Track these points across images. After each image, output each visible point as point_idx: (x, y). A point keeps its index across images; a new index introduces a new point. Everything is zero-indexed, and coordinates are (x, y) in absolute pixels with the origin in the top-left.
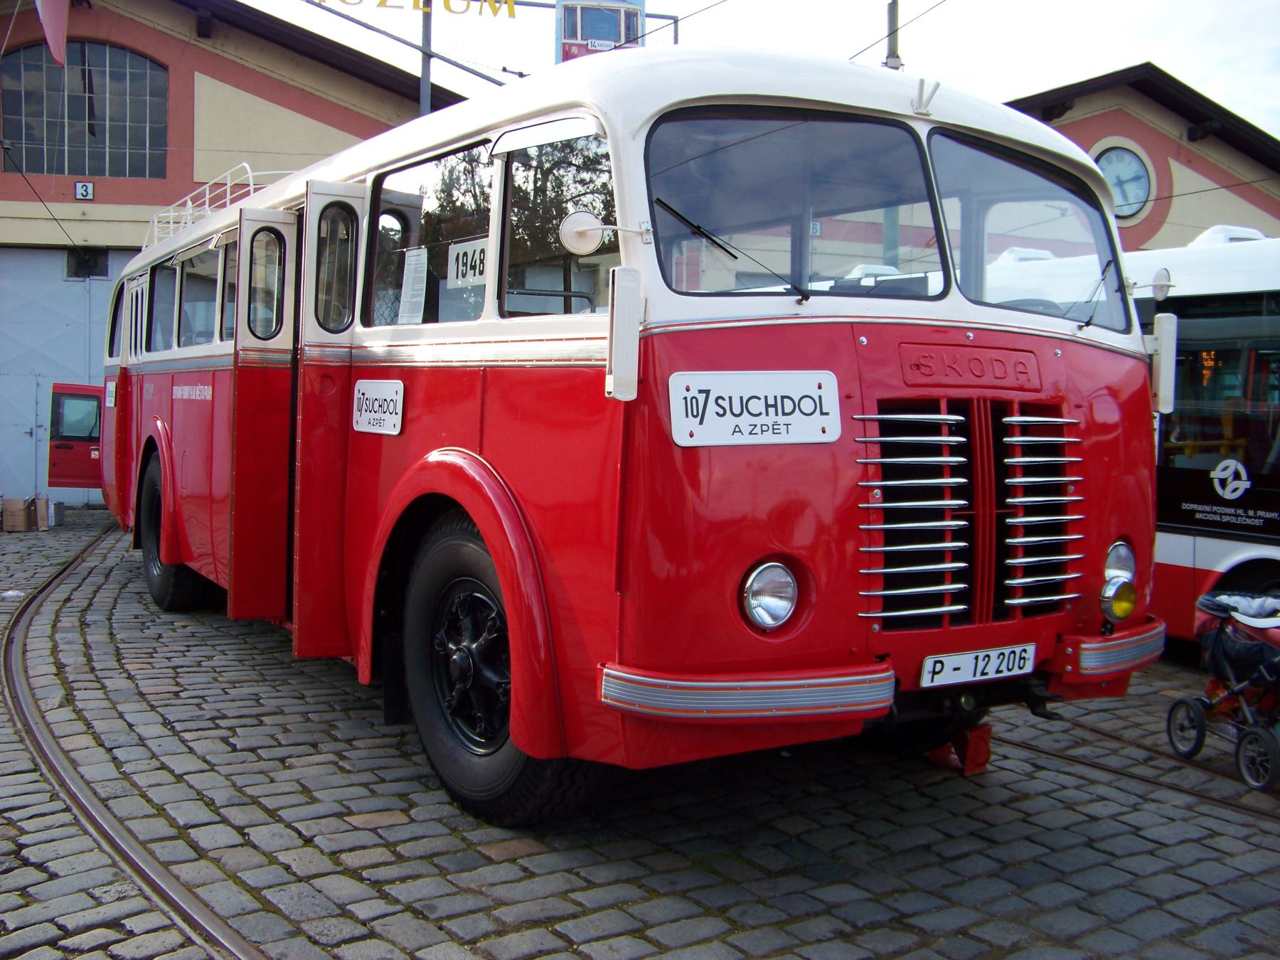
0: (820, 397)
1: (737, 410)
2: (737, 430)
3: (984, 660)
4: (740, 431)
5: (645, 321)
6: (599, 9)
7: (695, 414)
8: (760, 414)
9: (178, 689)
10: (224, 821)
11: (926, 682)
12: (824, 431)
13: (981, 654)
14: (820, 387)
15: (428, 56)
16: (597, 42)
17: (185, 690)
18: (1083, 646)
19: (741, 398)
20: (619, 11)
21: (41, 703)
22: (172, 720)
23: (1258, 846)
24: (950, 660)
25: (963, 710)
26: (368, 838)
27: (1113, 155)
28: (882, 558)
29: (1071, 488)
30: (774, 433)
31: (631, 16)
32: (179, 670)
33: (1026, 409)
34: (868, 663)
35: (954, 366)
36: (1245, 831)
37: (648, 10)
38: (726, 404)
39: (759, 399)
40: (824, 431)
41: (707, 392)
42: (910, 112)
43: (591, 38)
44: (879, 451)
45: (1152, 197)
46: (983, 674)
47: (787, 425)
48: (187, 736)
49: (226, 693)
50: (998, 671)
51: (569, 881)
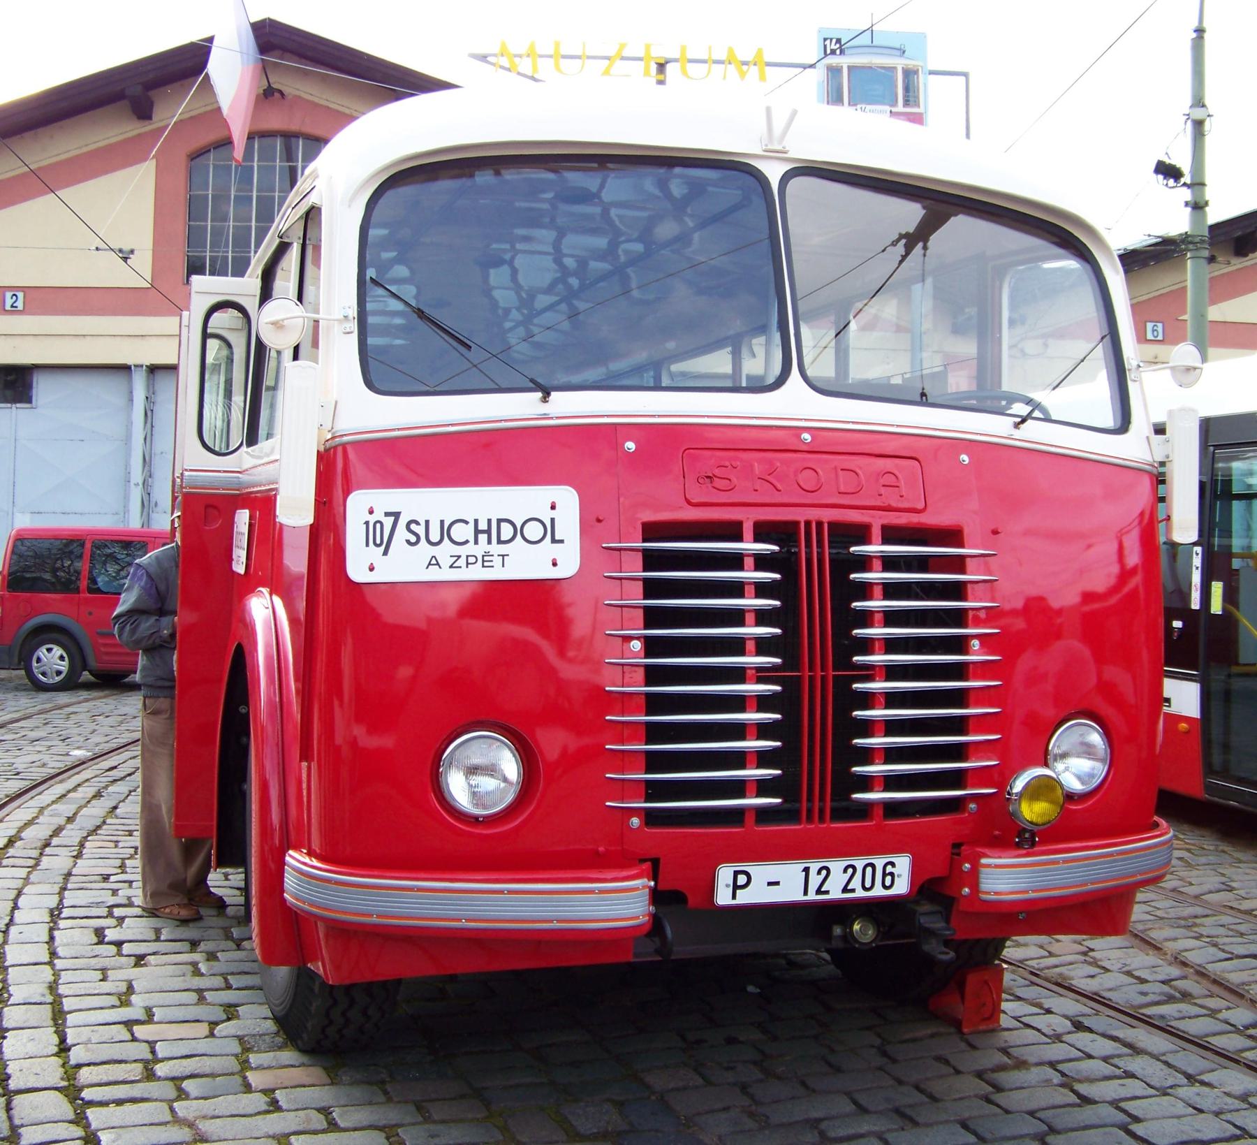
0: (553, 520)
1: (435, 537)
2: (434, 562)
3: (819, 872)
4: (438, 564)
5: (332, 428)
6: (870, 68)
7: (378, 542)
8: (467, 542)
11: (723, 897)
12: (555, 564)
13: (814, 866)
14: (553, 507)
18: (984, 861)
19: (442, 522)
20: (895, 68)
21: (242, 884)
24: (761, 872)
25: (856, 941)
28: (643, 731)
29: (975, 644)
30: (483, 566)
31: (909, 74)
33: (890, 536)
34: (622, 866)
35: (769, 478)
37: (932, 66)
38: (420, 530)
39: (466, 522)
40: (555, 564)
41: (396, 515)
42: (759, 151)
43: (860, 104)
44: (753, 591)
46: (819, 892)
47: (503, 556)
49: (227, 879)
50: (845, 890)
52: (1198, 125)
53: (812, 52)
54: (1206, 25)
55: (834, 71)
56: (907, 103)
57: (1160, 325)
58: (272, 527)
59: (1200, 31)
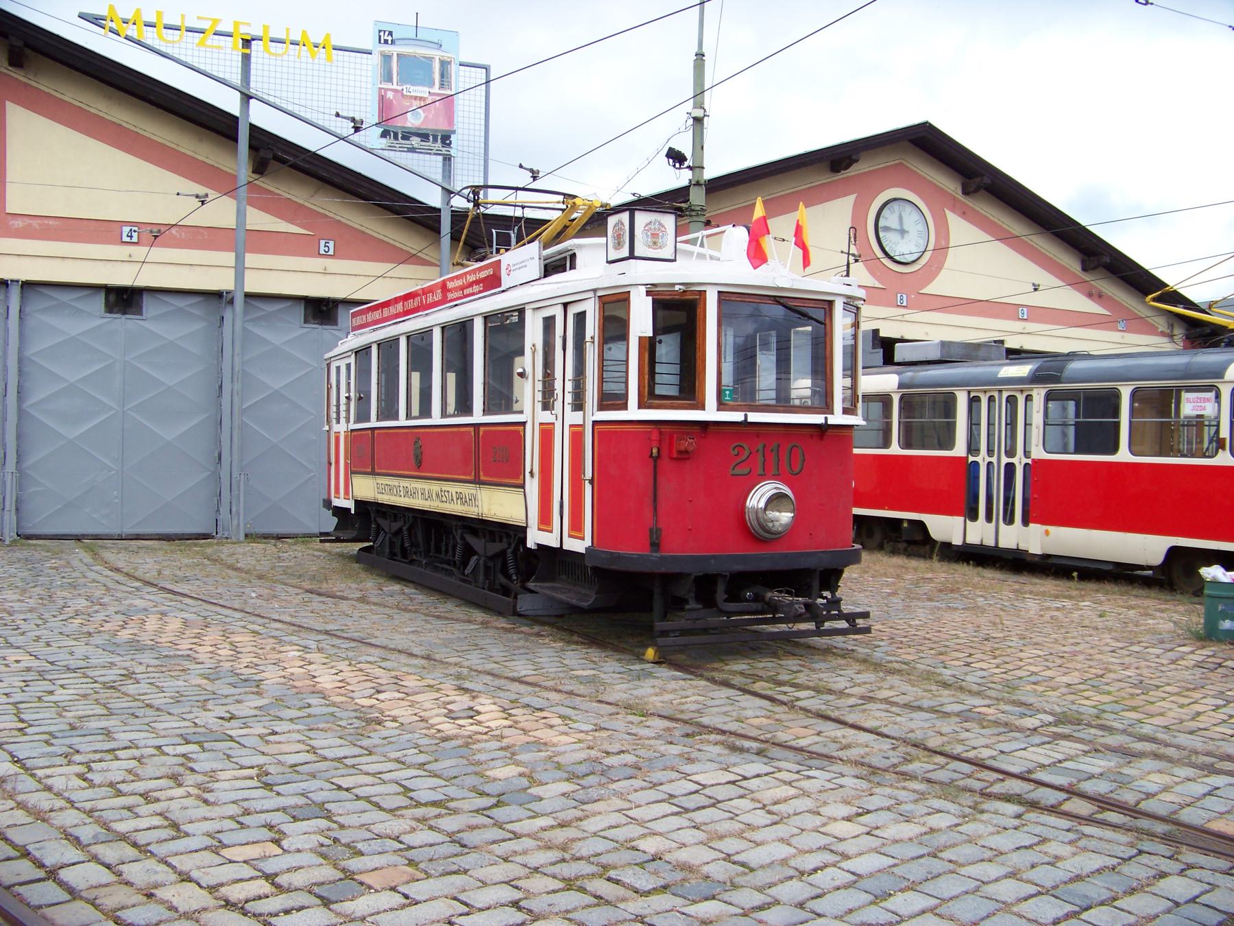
9: (21, 725)
10: (95, 858)
15: (247, 98)
16: (412, 88)
17: (31, 726)
22: (21, 758)
23: (1085, 849)
26: (247, 872)
27: (895, 205)
31: (444, 64)
32: (20, 706)
36: (1071, 836)
43: (406, 83)
45: (931, 247)
48: (40, 773)
51: (450, 906)
52: (698, 121)
53: (367, 40)
54: (704, 50)
55: (387, 58)
56: (442, 86)
57: (905, 296)
58: (496, 480)
59: (700, 55)
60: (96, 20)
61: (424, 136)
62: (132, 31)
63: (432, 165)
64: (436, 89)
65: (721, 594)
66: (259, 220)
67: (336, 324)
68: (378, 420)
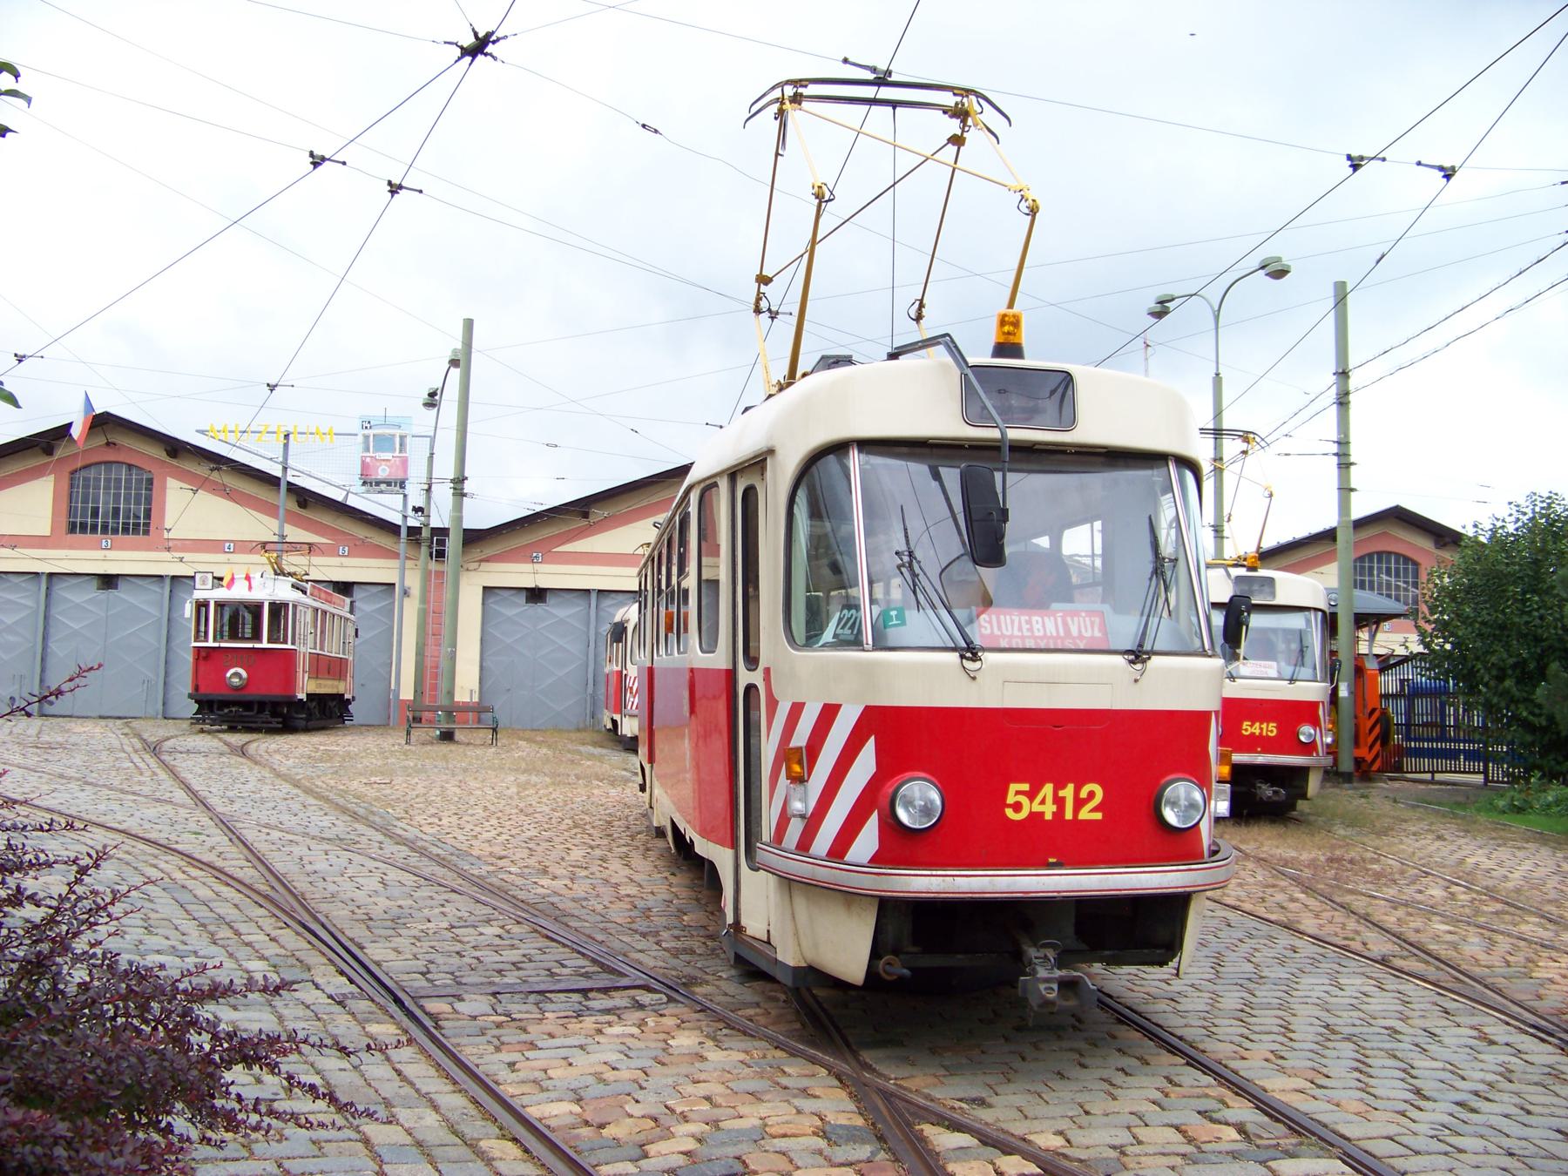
16: (382, 454)
31: (402, 438)
53: (355, 427)
55: (366, 437)
56: (401, 451)
60: (202, 432)
61: (389, 484)
62: (222, 436)
63: (395, 500)
64: (397, 454)
65: (215, 707)
66: (295, 534)
67: (545, 602)
68: (269, 642)
